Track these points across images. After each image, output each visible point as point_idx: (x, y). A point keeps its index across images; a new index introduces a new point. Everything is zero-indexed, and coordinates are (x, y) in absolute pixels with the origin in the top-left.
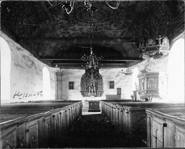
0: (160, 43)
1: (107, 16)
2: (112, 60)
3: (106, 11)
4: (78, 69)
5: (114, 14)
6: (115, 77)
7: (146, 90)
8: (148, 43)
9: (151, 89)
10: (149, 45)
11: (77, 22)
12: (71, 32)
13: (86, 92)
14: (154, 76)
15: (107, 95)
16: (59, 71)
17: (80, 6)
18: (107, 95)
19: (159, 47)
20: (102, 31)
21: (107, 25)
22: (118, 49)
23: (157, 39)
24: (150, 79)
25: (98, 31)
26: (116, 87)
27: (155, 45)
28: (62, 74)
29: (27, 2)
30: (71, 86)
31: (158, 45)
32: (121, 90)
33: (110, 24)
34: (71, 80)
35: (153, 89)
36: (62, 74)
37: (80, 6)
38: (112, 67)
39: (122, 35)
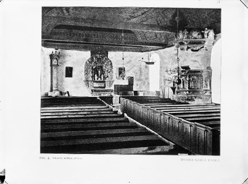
0: (205, 37)
7: (188, 90)
8: (191, 35)
9: (193, 89)
10: (193, 37)
13: (91, 81)
14: (197, 74)
15: (115, 86)
16: (54, 53)
18: (115, 86)
19: (204, 42)
23: (203, 32)
24: (192, 77)
26: (128, 74)
27: (201, 38)
28: (59, 56)
29: (152, 10)
30: (69, 72)
31: (204, 40)
32: (133, 79)
34: (69, 65)
35: (196, 89)
36: (59, 56)
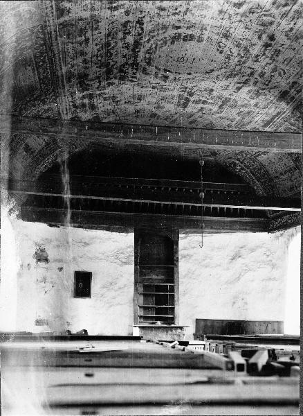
1: (237, 59)
2: (227, 206)
3: (238, 46)
4: (105, 232)
5: (264, 54)
6: (226, 261)
11: (134, 73)
12: (103, 106)
17: (161, 23)
20: (202, 108)
21: (226, 88)
22: (242, 169)
33: (239, 89)
37: (161, 23)
38: (246, 230)
39: (265, 126)
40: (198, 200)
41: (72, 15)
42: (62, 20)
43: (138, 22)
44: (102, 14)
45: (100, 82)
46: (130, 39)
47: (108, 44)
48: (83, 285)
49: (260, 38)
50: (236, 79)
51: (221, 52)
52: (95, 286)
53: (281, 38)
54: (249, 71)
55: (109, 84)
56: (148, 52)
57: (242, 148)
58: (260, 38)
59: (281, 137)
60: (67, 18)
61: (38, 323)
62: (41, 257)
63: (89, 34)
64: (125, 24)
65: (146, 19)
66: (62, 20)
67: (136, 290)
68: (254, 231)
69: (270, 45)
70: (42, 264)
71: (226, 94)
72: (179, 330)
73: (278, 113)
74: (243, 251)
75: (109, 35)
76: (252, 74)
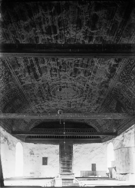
25: (72, 107)
40: (64, 134)
41: (26, 83)
42: (23, 85)
43: (47, 84)
44: (35, 83)
45: (42, 101)
46: (46, 89)
47: (40, 91)
48: (45, 161)
49: (84, 85)
50: (82, 98)
51: (75, 90)
52: (49, 161)
53: (90, 85)
54: (85, 95)
55: (45, 102)
56: (53, 92)
57: (90, 118)
58: (84, 85)
59: (89, 114)
60: (24, 84)
61: (31, 173)
62: (32, 153)
63: (33, 88)
64: (43, 85)
65: (49, 83)
66: (23, 85)
67: (60, 162)
68: (97, 143)
69: (88, 87)
70: (32, 155)
71: (81, 102)
72: (73, 175)
73: (98, 107)
74: (94, 149)
75: (39, 88)
76: (86, 96)
